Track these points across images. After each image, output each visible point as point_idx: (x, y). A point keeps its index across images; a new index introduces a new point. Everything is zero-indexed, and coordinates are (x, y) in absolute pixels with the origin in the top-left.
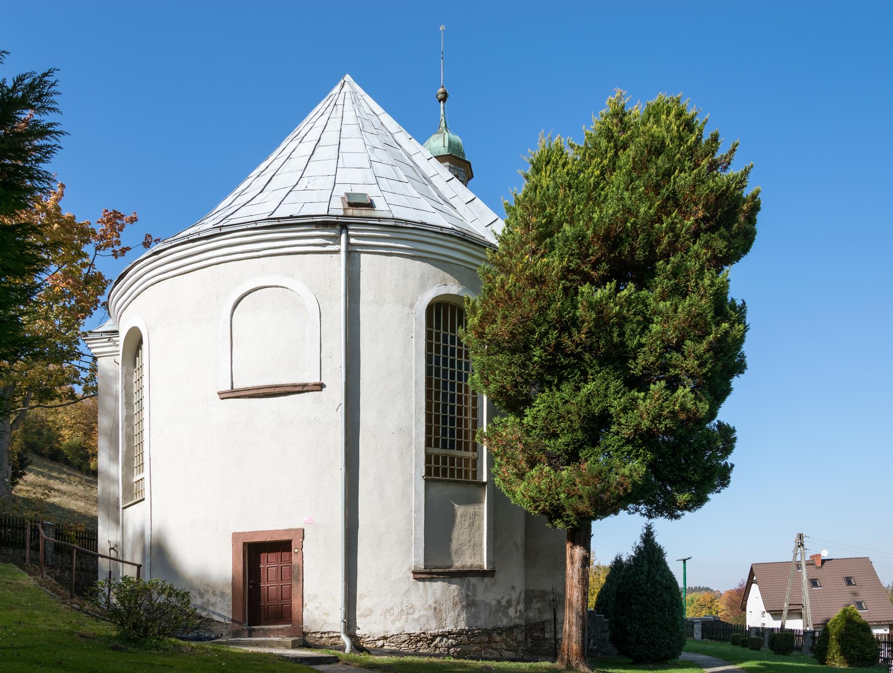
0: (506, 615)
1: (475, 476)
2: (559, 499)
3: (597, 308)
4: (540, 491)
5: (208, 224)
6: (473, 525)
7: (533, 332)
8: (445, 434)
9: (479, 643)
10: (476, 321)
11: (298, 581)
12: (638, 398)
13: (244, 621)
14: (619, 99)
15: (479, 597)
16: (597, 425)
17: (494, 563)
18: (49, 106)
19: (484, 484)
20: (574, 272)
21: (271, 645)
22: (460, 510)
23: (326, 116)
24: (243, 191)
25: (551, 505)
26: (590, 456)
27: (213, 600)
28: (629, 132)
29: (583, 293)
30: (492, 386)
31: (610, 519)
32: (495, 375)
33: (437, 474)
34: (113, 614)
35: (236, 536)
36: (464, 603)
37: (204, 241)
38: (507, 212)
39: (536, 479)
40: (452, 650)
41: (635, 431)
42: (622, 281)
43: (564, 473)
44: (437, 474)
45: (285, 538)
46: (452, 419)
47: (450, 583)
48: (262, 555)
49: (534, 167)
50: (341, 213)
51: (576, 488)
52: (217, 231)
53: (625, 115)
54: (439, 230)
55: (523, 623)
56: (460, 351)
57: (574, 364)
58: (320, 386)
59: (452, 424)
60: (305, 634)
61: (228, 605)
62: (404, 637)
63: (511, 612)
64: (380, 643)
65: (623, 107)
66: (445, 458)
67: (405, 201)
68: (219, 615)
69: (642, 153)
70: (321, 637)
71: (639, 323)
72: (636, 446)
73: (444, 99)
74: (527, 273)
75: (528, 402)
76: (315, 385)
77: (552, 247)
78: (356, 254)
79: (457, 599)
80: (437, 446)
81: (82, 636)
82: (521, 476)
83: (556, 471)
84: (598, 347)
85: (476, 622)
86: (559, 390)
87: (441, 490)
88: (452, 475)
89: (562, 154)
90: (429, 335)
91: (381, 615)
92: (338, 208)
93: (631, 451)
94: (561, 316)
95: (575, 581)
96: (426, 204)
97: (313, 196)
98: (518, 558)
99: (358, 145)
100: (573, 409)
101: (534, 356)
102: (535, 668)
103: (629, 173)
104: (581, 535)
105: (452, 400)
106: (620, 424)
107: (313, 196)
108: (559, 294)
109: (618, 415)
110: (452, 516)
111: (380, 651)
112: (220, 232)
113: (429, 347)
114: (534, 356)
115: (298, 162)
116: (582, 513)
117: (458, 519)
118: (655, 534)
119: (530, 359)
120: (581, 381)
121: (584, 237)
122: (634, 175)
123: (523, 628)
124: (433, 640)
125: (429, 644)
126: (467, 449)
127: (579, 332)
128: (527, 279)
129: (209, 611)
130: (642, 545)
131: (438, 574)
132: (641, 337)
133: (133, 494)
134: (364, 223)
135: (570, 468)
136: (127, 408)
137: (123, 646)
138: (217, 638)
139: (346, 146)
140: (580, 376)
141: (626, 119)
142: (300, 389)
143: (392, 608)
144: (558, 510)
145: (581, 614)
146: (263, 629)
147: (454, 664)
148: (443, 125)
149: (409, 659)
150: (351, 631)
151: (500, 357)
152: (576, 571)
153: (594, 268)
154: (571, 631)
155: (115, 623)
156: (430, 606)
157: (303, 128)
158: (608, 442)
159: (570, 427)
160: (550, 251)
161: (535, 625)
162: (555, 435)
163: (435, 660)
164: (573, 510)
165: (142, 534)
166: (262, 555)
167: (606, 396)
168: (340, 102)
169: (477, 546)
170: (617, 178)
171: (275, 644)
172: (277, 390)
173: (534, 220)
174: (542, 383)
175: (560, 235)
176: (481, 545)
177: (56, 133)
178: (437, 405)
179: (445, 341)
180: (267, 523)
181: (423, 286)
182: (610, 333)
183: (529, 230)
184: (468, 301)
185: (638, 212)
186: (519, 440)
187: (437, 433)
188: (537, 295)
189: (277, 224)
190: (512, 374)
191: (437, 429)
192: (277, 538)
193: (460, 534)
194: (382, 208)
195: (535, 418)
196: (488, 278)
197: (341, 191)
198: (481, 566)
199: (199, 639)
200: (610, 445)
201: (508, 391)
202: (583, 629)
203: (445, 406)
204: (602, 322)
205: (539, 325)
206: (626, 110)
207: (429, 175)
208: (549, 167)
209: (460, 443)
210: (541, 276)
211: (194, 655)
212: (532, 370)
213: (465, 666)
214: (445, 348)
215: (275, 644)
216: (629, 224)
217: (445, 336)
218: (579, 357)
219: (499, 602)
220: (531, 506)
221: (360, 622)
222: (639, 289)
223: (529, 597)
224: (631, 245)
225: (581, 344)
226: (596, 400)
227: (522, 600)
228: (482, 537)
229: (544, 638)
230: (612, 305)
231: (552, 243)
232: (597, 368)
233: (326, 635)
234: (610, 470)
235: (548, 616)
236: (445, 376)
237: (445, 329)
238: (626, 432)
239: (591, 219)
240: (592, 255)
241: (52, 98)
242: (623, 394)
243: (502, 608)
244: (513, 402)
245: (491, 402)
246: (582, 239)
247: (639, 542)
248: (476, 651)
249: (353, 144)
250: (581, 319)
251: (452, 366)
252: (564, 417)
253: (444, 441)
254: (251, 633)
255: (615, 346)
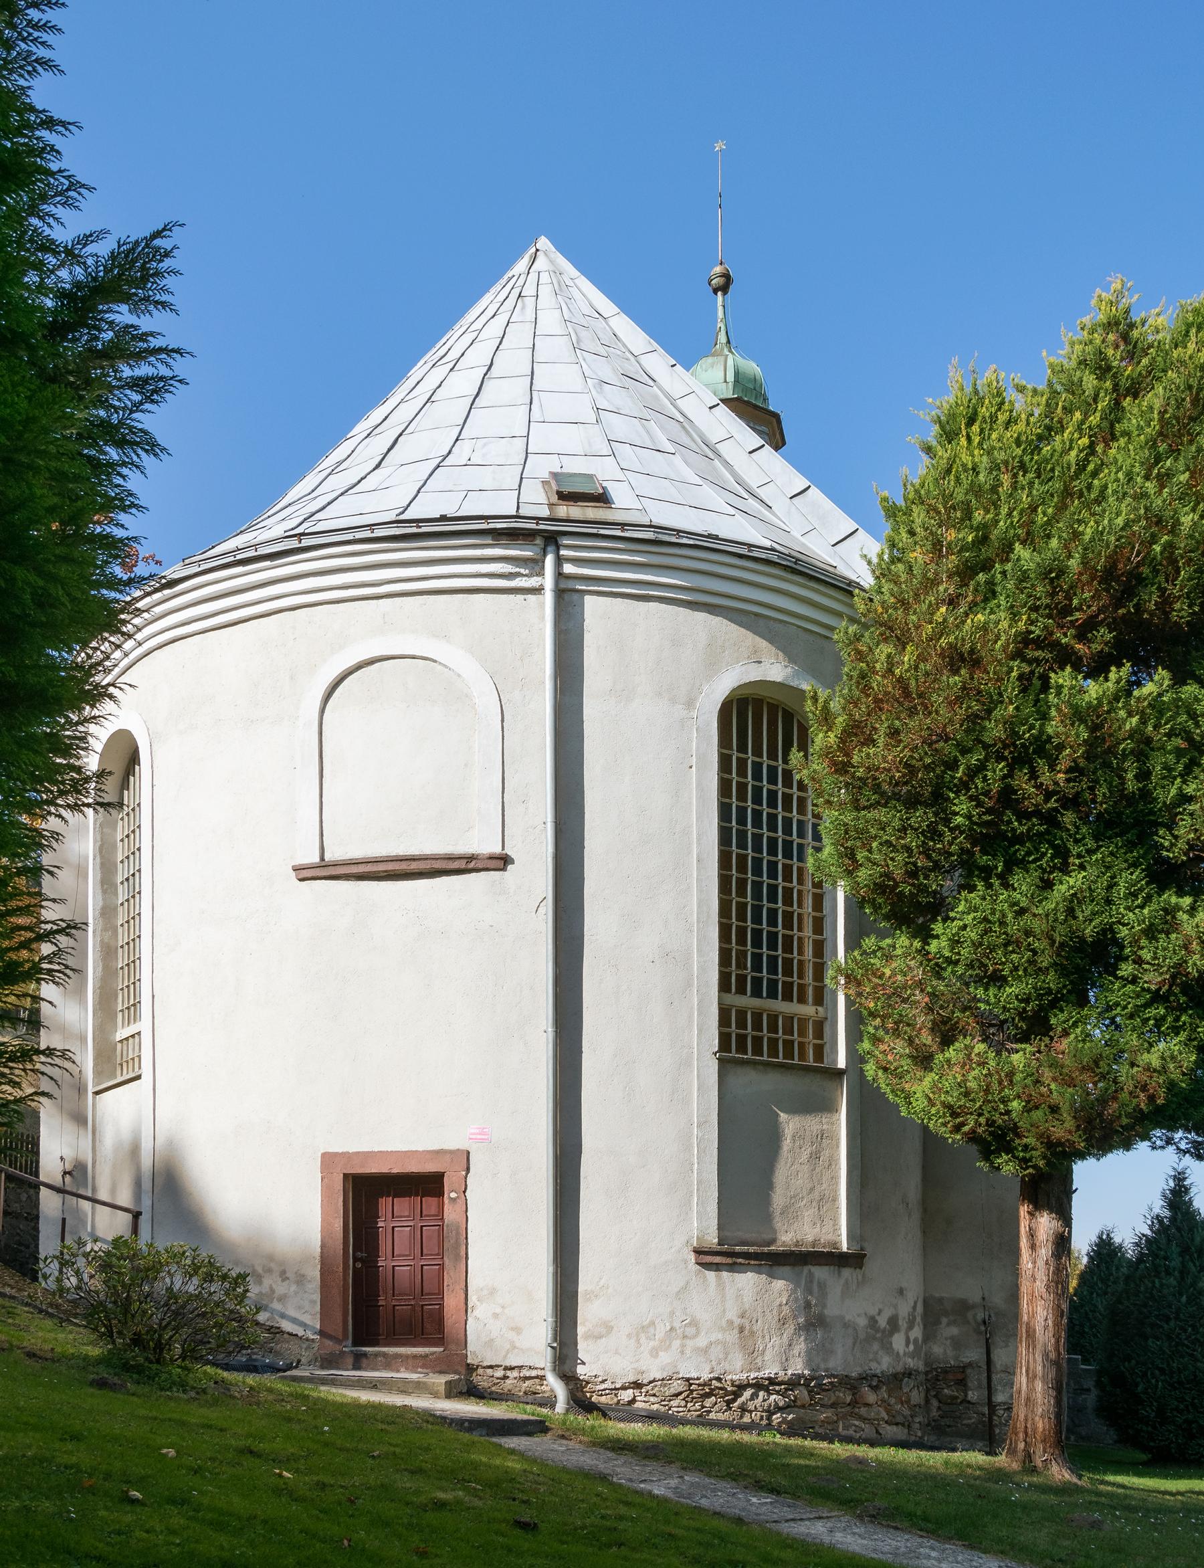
0: (888, 1348)
1: (819, 1052)
2: (1008, 1112)
3: (1091, 718)
4: (966, 1094)
5: (272, 528)
6: (819, 1156)
7: (953, 765)
8: (757, 967)
9: (833, 1405)
10: (832, 738)
11: (457, 1257)
12: (1178, 908)
13: (345, 1337)
14: (1119, 294)
15: (833, 1309)
16: (1089, 960)
17: (862, 1239)
18: (158, 297)
19: (840, 1073)
20: (1038, 643)
21: (404, 1388)
22: (790, 1124)
23: (502, 319)
24: (340, 463)
25: (990, 1123)
26: (1075, 1025)
27: (281, 1289)
28: (1145, 361)
29: (1059, 688)
30: (863, 874)
31: (1116, 1159)
32: (870, 851)
33: (742, 1048)
34: (91, 1312)
35: (328, 1160)
36: (801, 1320)
37: (267, 563)
38: (888, 517)
39: (957, 1069)
40: (777, 1418)
41: (1174, 977)
42: (1144, 666)
43: (1015, 1058)
44: (742, 1048)
45: (431, 1167)
46: (773, 937)
47: (772, 1276)
48: (382, 1201)
49: (942, 427)
50: (545, 512)
51: (1044, 1090)
52: (294, 544)
53: (1132, 326)
54: (745, 552)
55: (921, 1366)
56: (787, 799)
57: (1039, 834)
58: (502, 861)
59: (773, 946)
60: (471, 1369)
61: (313, 1302)
62: (678, 1386)
63: (898, 1342)
64: (626, 1395)
65: (1127, 312)
66: (757, 1017)
67: (671, 492)
68: (294, 1321)
69: (1180, 403)
70: (505, 1377)
71: (1179, 753)
72: (1173, 1009)
73: (724, 288)
74: (943, 642)
75: (938, 908)
76: (492, 857)
77: (990, 593)
78: (575, 596)
79: (786, 1310)
80: (741, 990)
81: (31, 1355)
82: (924, 1060)
83: (998, 1053)
84: (1094, 801)
85: (825, 1360)
86: (1006, 886)
87: (751, 1082)
88: (773, 1052)
89: (1003, 403)
90: (724, 763)
91: (629, 1336)
92: (537, 503)
93: (1163, 1018)
94: (1014, 734)
95: (1040, 1285)
96: (717, 500)
97: (485, 478)
98: (908, 1230)
99: (569, 376)
100: (1037, 925)
101: (957, 814)
102: (956, 1465)
103: (1152, 443)
104: (1050, 1190)
105: (773, 898)
106: (1139, 961)
107: (485, 478)
108: (1011, 689)
109: (1135, 942)
110: (773, 1138)
111: (627, 1412)
112: (298, 545)
113: (724, 787)
114: (957, 814)
115: (450, 410)
116: (1059, 1143)
117: (787, 1144)
118: (1193, 1191)
119: (947, 821)
120: (1054, 869)
121: (1062, 572)
122: (1162, 447)
123: (922, 1378)
124: (737, 1395)
125: (728, 1403)
126: (802, 1000)
127: (1052, 768)
128: (942, 655)
129: (273, 1311)
130: (1166, 1213)
131: (747, 1256)
132: (1184, 782)
133: (117, 1066)
134: (593, 532)
135: (1029, 1048)
136: (104, 892)
137: (116, 1380)
138: (289, 1367)
139: (541, 378)
140: (1052, 858)
141: (1135, 333)
142: (461, 864)
143: (652, 1323)
144: (1004, 1135)
145: (1053, 1356)
146: (385, 1355)
147: (788, 1450)
148: (722, 338)
149: (689, 1432)
150: (566, 1368)
151: (880, 814)
152: (1041, 1263)
153: (1081, 636)
154: (1031, 1389)
155: (95, 1330)
156: (730, 1322)
157: (455, 340)
158: (1113, 999)
159: (1031, 962)
160: (986, 600)
161: (945, 1371)
162: (997, 979)
163: (746, 1437)
164: (1040, 1136)
165: (135, 1151)
166: (382, 1201)
167: (1109, 902)
168: (529, 290)
169: (826, 1201)
170: (1124, 456)
171: (402, 1386)
172: (414, 866)
173: (951, 535)
174: (971, 872)
175: (1008, 567)
176: (835, 1199)
177: (160, 350)
178: (742, 908)
179: (757, 776)
180: (395, 1135)
181: (712, 666)
182: (1120, 773)
183: (941, 556)
184: (815, 699)
185: (1177, 523)
186: (920, 984)
187: (741, 965)
188: (964, 688)
189: (414, 533)
190: (908, 849)
191: (742, 955)
192: (414, 1167)
193: (790, 1175)
194: (627, 502)
195: (955, 942)
196: (859, 652)
197: (541, 468)
198: (835, 1244)
199: (251, 1368)
200: (1117, 1004)
201: (896, 885)
202: (1058, 1388)
203: (757, 910)
204: (1100, 751)
205: (965, 751)
206: (1136, 318)
207: (713, 439)
208: (976, 428)
209: (788, 987)
210: (972, 651)
211: (258, 1404)
212: (951, 844)
213: (811, 1454)
214: (757, 791)
215: (402, 1386)
216: (1157, 548)
217: (757, 767)
218: (1051, 819)
219: (873, 1321)
220: (945, 1125)
221: (584, 1349)
222: (1179, 680)
223: (933, 1312)
224: (1162, 590)
225: (1055, 793)
226: (1088, 909)
227: (918, 1319)
228: (837, 1184)
229: (965, 1401)
230: (1122, 714)
231: (991, 583)
232: (1091, 844)
233: (515, 1374)
234: (1117, 1058)
235: (974, 1354)
236: (757, 848)
237: (758, 752)
238: (1152, 979)
239: (1076, 535)
240: (1079, 609)
241: (164, 282)
242: (1148, 899)
243: (879, 1333)
244: (907, 908)
245: (855, 905)
246: (1058, 577)
247: (1159, 1207)
248: (827, 1422)
249: (561, 374)
250: (1056, 741)
251: (773, 827)
252: (1018, 943)
253: (757, 982)
254: (358, 1362)
255: (1130, 800)
